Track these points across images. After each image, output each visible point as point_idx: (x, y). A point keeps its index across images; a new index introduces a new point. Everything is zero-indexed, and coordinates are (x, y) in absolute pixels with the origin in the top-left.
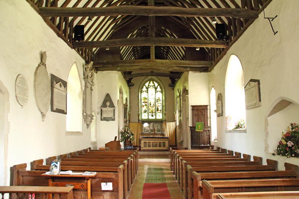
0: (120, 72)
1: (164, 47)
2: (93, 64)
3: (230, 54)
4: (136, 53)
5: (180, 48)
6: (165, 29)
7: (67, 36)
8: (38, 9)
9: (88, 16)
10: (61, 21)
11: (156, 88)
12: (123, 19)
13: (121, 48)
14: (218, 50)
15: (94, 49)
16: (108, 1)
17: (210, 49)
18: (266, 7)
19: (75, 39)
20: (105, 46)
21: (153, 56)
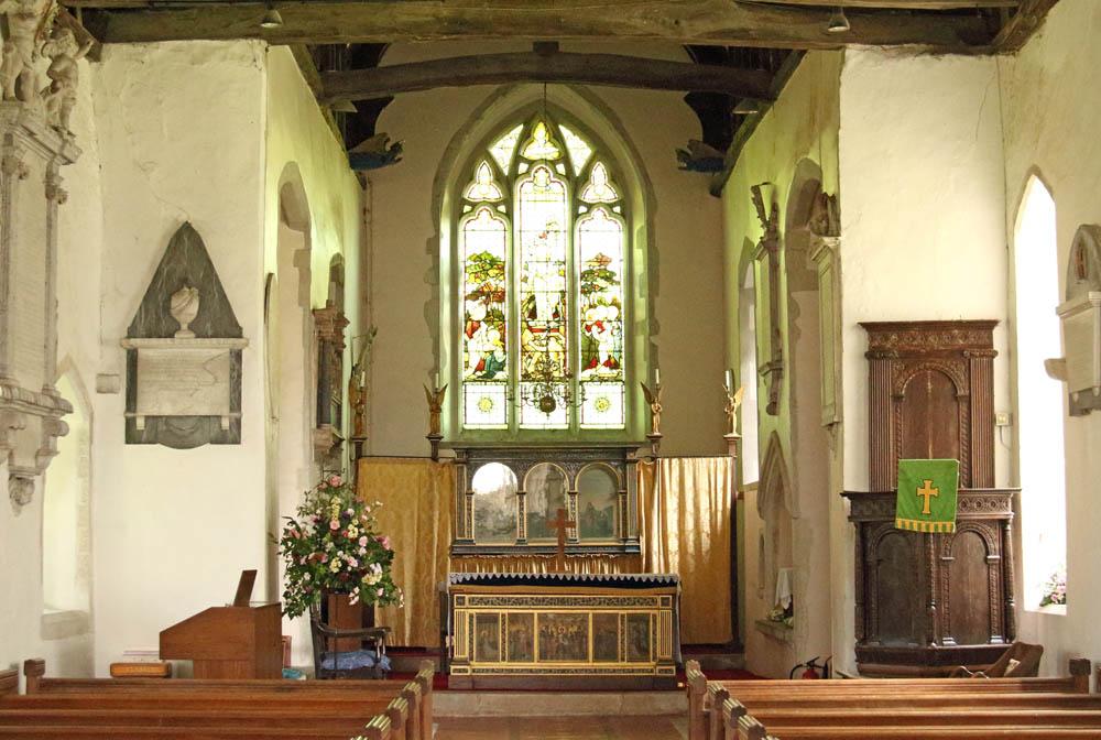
11: (577, 183)
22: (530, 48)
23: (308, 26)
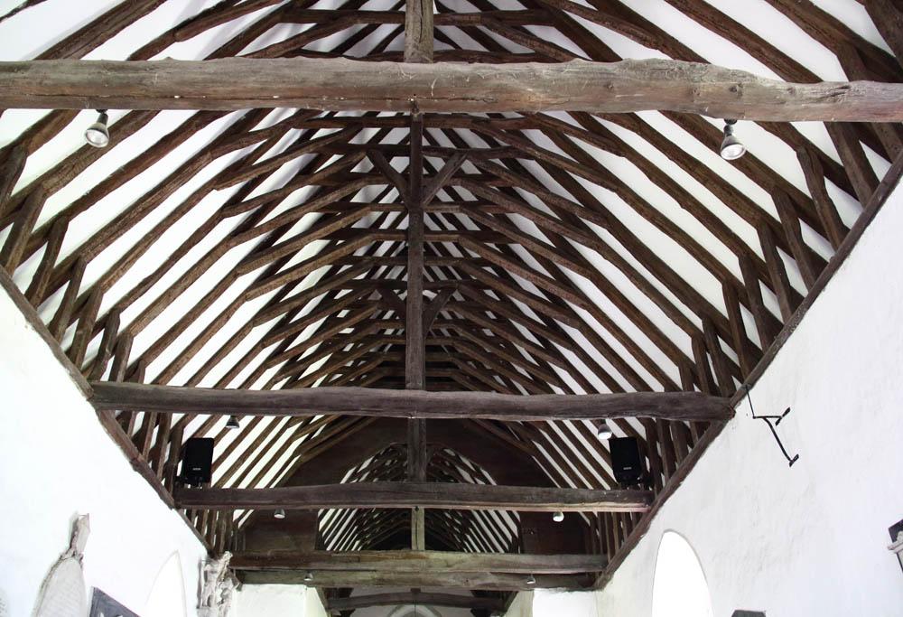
0: (314, 589)
1: (453, 512)
2: (231, 559)
3: (662, 532)
4: (375, 516)
5: (505, 517)
6: (457, 456)
7: (160, 470)
8: (87, 385)
9: (227, 412)
10: (148, 424)
12: (331, 425)
13: (320, 513)
14: (623, 517)
15: (237, 513)
16: (291, 372)
17: (596, 514)
18: (752, 385)
19: (182, 480)
20: (273, 507)
21: (419, 540)
22: (409, 590)
23: (323, 580)
